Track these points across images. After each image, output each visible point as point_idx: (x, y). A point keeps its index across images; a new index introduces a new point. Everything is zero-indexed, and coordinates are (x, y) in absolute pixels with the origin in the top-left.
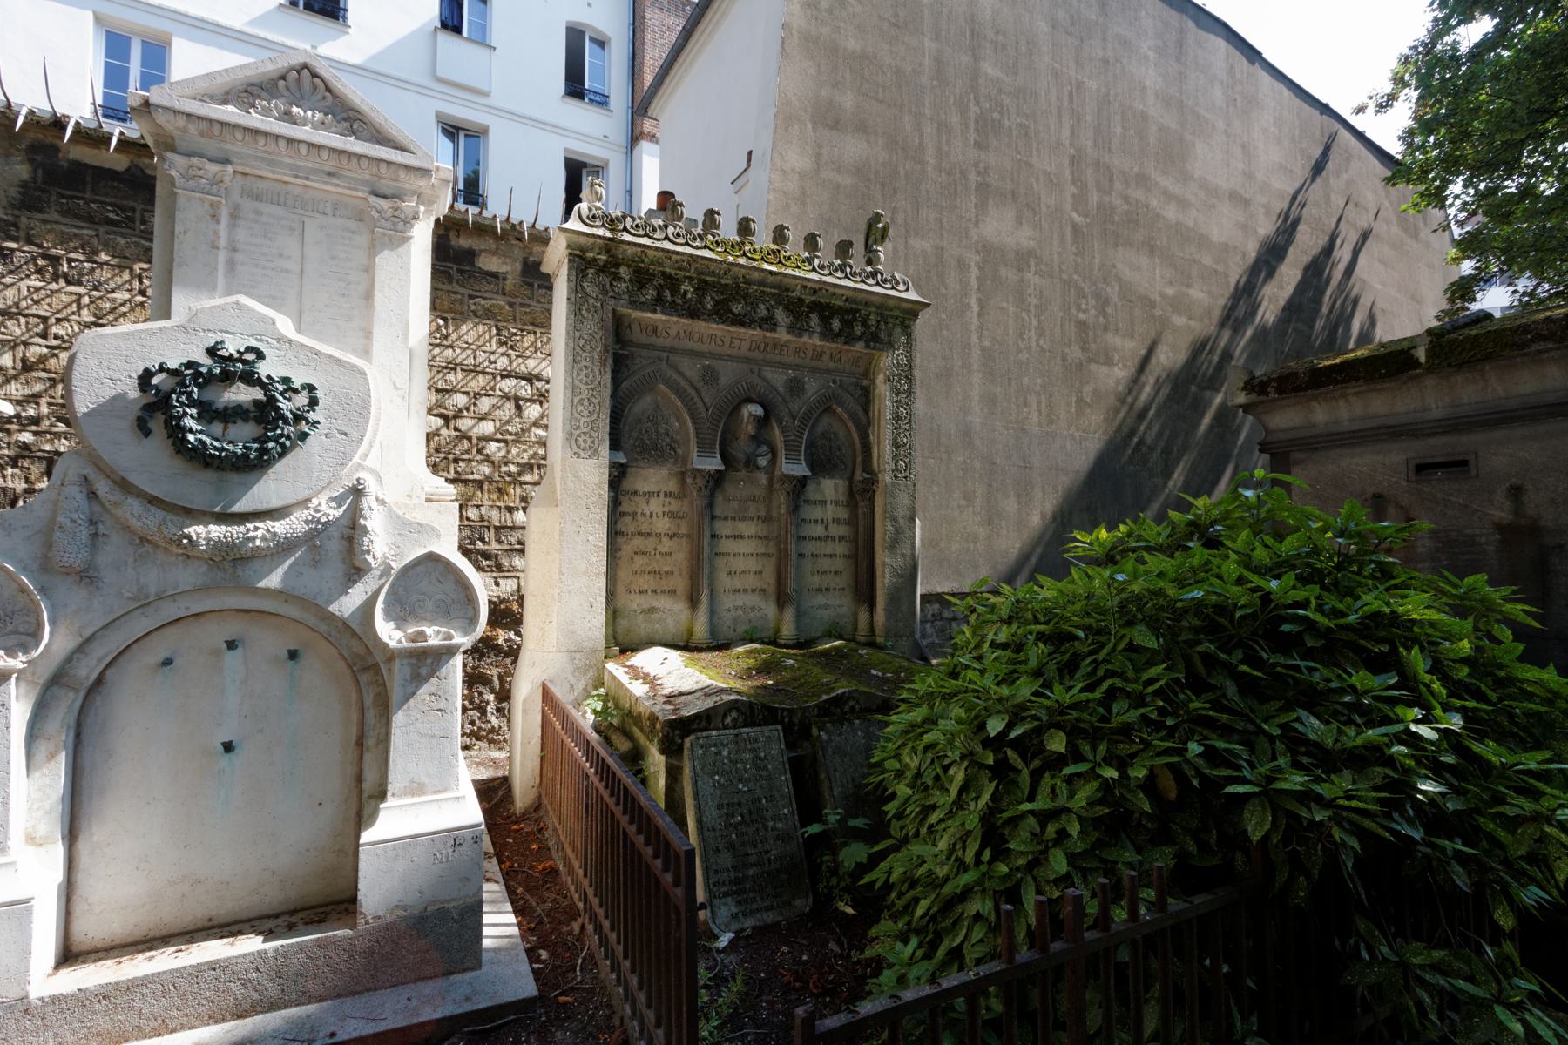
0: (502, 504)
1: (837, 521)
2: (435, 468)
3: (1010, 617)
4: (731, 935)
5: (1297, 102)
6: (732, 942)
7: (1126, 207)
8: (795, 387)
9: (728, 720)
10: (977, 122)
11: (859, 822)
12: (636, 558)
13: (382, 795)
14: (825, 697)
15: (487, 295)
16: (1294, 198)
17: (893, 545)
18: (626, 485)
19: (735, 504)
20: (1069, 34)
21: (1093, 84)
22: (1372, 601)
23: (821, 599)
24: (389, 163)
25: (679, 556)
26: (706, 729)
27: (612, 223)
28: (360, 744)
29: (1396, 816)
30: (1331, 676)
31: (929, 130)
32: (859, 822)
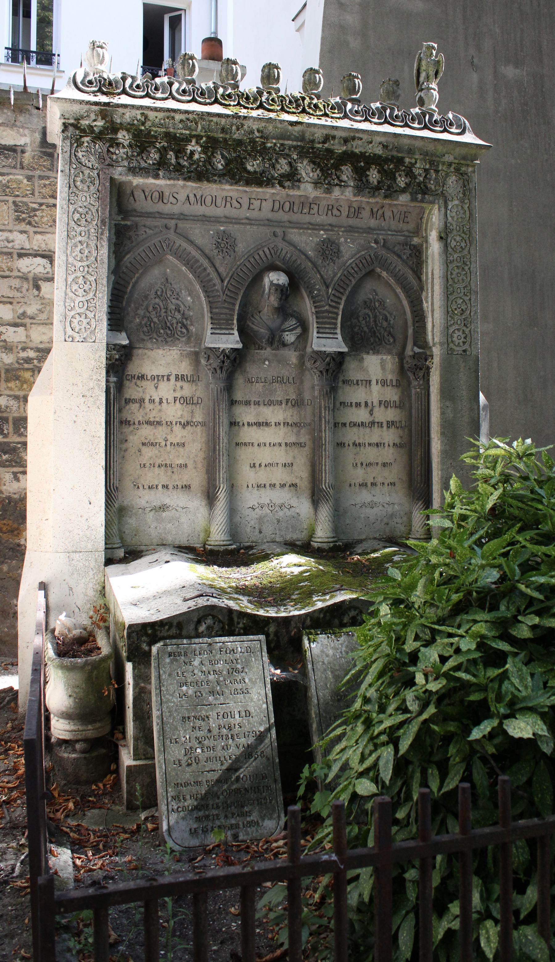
8: (329, 250)
12: (144, 449)
18: (133, 368)
19: (259, 387)
23: (365, 496)
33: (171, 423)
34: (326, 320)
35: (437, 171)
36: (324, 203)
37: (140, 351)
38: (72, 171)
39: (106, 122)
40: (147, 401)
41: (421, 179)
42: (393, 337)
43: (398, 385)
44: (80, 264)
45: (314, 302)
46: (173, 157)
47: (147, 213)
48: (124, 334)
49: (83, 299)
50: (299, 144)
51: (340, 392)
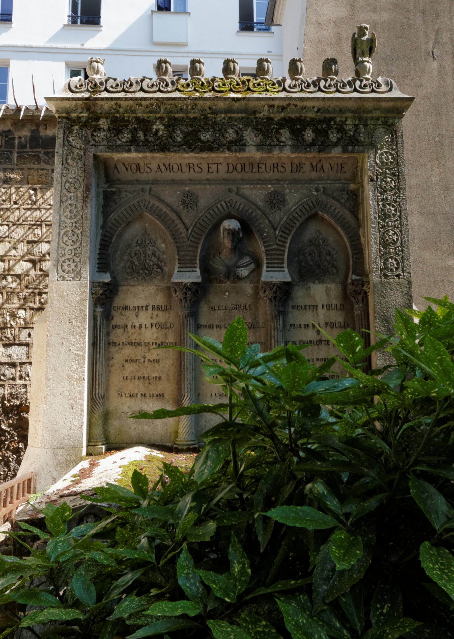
1: (330, 325)
8: (276, 200)
12: (127, 365)
18: (118, 301)
19: (221, 313)
33: (149, 344)
34: (275, 256)
35: (366, 125)
36: (269, 162)
37: (125, 288)
38: (65, 152)
39: (90, 113)
40: (129, 326)
41: (352, 133)
42: (336, 268)
43: (342, 308)
44: (70, 221)
45: (264, 243)
46: (142, 135)
47: (128, 181)
48: (108, 275)
49: (71, 248)
50: (244, 115)
51: (290, 315)
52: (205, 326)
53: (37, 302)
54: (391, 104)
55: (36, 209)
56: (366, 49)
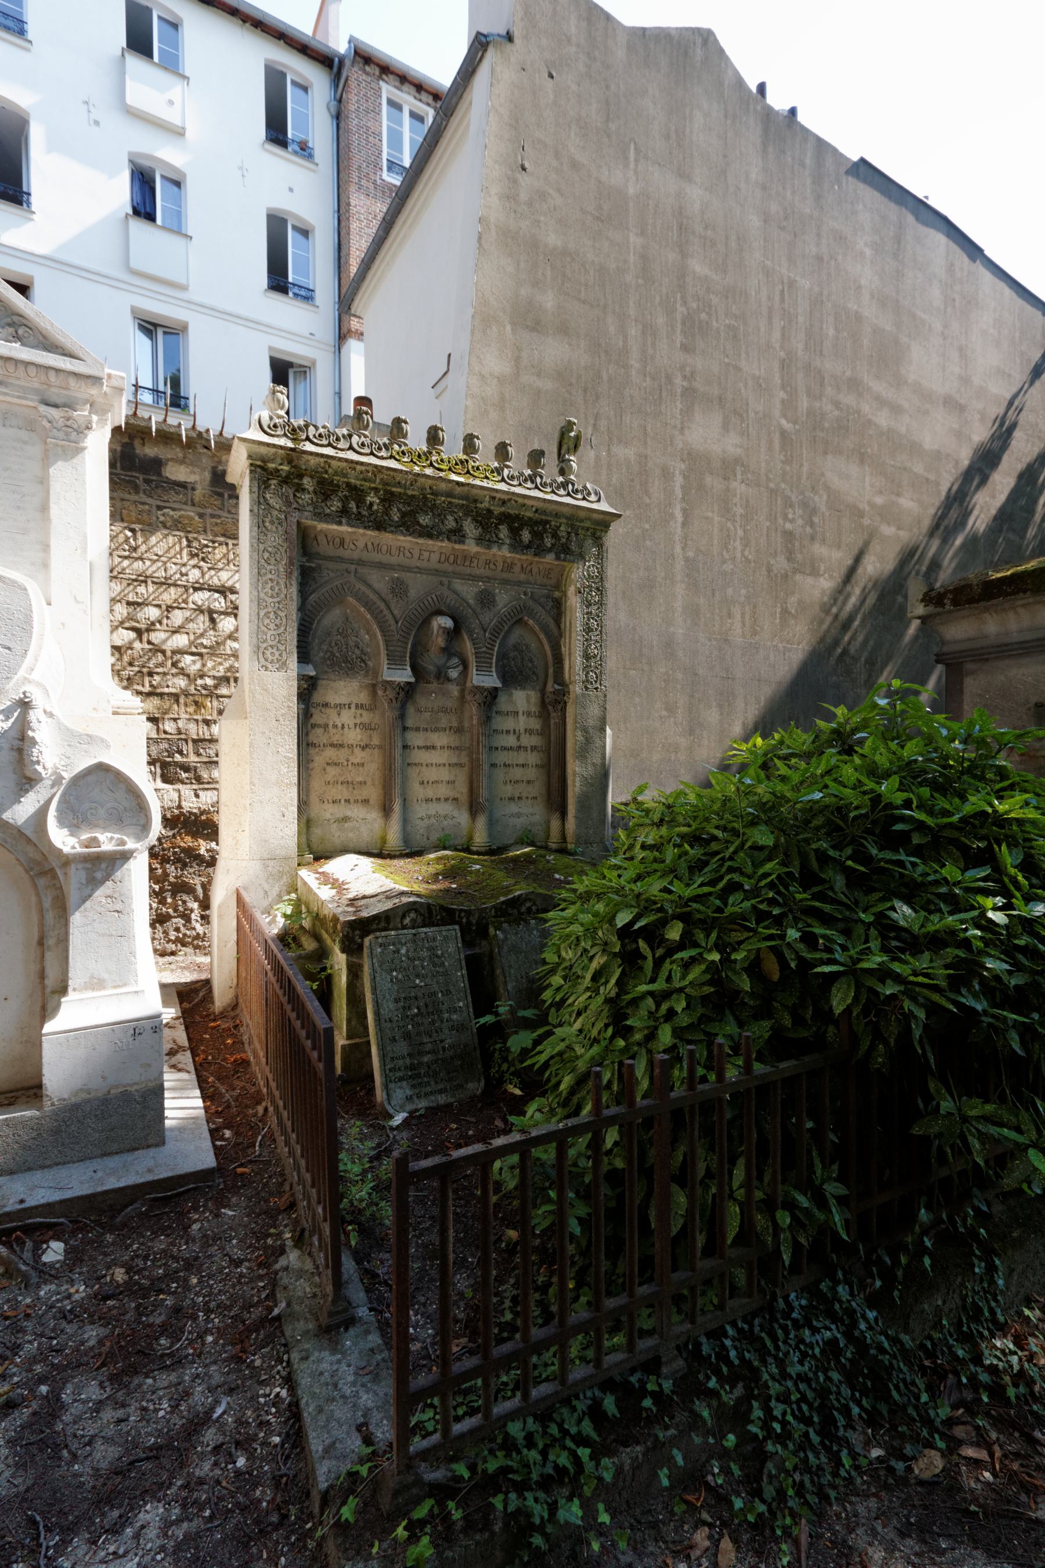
0: (199, 717)
1: (530, 732)
2: (128, 683)
3: (662, 820)
4: (405, 1115)
5: (1020, 302)
6: (406, 1121)
7: (836, 413)
8: (486, 599)
9: (407, 921)
10: (683, 323)
11: (528, 1013)
12: (329, 769)
13: (63, 990)
14: (502, 899)
15: (175, 506)
16: (1011, 403)
17: (583, 753)
18: (317, 697)
20: (783, 228)
21: (805, 283)
22: (975, 802)
23: (513, 808)
24: (58, 371)
25: (372, 765)
26: (385, 929)
27: (294, 433)
28: (41, 943)
29: (964, 991)
30: (927, 870)
31: (633, 331)
32: (528, 1013)
35: (577, 534)
36: (484, 557)
52: (411, 729)
53: (147, 685)
54: (601, 517)
55: (137, 559)
56: (572, 446)
